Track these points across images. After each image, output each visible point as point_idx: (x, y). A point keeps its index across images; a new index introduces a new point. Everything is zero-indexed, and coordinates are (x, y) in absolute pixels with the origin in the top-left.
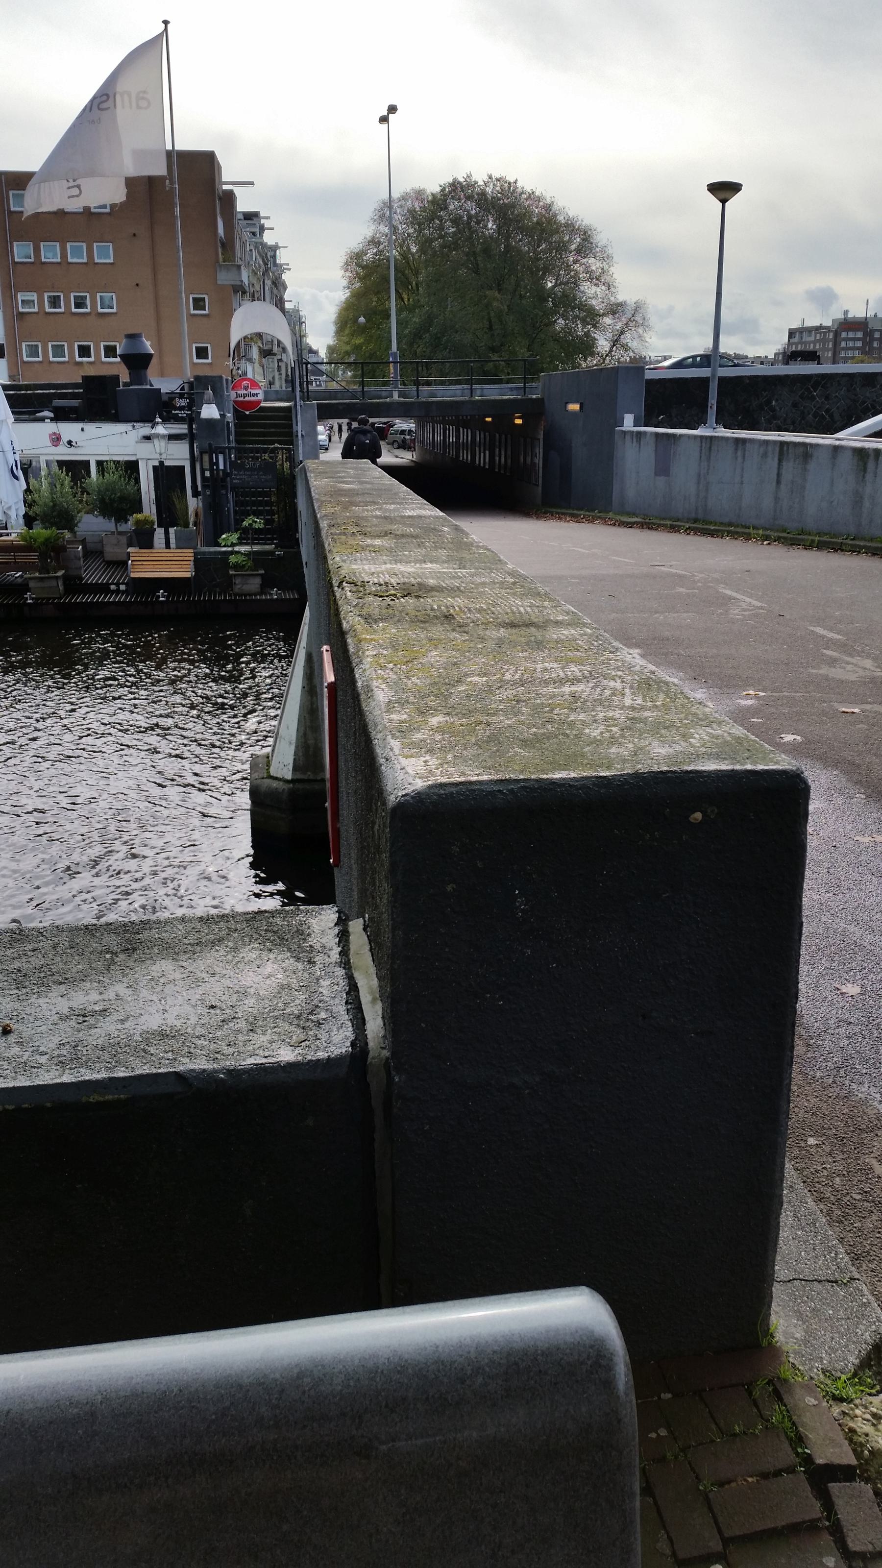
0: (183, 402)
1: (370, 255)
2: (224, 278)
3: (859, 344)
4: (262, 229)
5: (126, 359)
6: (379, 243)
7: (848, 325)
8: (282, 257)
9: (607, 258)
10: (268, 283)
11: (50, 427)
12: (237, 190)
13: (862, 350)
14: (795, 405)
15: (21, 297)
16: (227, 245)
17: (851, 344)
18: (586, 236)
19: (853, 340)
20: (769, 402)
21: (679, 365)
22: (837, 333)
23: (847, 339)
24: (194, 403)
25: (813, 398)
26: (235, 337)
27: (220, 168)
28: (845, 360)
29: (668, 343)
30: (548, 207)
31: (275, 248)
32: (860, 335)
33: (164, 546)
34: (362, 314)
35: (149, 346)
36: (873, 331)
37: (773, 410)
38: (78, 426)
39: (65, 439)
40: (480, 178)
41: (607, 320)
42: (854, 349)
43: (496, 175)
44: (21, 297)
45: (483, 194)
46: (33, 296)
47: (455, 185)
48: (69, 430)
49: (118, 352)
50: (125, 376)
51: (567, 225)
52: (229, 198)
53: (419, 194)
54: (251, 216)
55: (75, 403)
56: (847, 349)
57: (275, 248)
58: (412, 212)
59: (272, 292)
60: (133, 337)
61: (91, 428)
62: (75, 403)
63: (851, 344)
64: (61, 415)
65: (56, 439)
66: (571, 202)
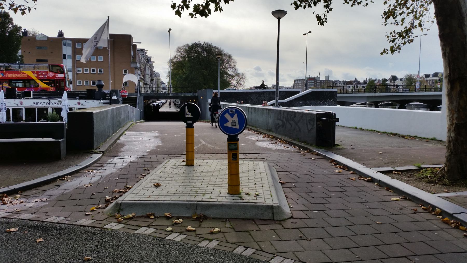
0: (108, 95)
1: (175, 60)
2: (133, 66)
3: (313, 84)
4: (146, 53)
5: (98, 86)
6: (177, 57)
7: (310, 79)
8: (152, 60)
9: (235, 63)
10: (147, 66)
11: (77, 101)
12: (137, 44)
13: (314, 85)
14: (257, 98)
15: (77, 69)
16: (134, 58)
17: (311, 84)
18: (230, 57)
19: (311, 83)
21: (251, 89)
22: (307, 81)
23: (310, 83)
24: (111, 95)
26: (124, 81)
27: (133, 38)
28: (296, 88)
29: (250, 83)
30: (220, 50)
31: (150, 58)
32: (313, 81)
33: (225, 190)
34: (173, 75)
35: (103, 83)
36: (317, 80)
38: (84, 101)
39: (81, 103)
40: (202, 43)
41: (236, 78)
42: (312, 85)
43: (206, 42)
44: (77, 69)
45: (203, 46)
46: (81, 69)
47: (195, 44)
48: (82, 101)
49: (96, 83)
50: (97, 89)
51: (224, 54)
52: (135, 46)
53: (188, 45)
54: (142, 50)
55: (84, 95)
56: (310, 85)
57: (150, 58)
58: (186, 50)
59: (148, 68)
60: (99, 81)
61: (88, 101)
62: (84, 95)
63: (311, 84)
64: (81, 98)
65: (79, 103)
66: (226, 50)
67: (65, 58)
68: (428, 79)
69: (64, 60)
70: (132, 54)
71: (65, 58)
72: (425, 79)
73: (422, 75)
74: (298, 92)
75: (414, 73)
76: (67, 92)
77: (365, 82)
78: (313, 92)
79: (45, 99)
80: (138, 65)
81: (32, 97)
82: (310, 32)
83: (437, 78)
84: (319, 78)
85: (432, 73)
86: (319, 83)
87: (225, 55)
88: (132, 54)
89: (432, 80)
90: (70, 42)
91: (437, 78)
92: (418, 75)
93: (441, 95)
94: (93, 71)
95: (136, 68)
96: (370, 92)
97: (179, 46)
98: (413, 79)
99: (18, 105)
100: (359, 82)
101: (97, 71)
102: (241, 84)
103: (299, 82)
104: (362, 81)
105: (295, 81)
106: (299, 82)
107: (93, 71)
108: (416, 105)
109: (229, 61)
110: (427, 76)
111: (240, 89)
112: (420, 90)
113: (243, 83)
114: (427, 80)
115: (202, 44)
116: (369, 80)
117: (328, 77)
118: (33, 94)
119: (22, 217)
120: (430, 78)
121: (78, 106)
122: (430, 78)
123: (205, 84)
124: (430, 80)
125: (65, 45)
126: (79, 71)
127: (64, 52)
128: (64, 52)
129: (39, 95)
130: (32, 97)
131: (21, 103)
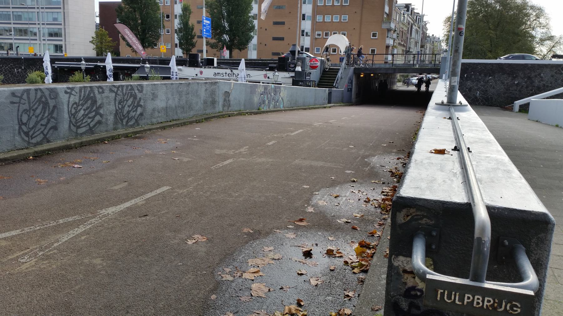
11: (264, 72)
14: (552, 76)
16: (389, 15)
20: (539, 74)
37: (542, 78)
41: (548, 42)
46: (321, 33)
48: (270, 74)
55: (275, 65)
62: (275, 65)
64: (271, 69)
67: (304, 19)
69: (303, 22)
70: (387, 10)
71: (304, 19)
76: (245, 60)
79: (227, 69)
80: (393, 26)
81: (215, 65)
87: (532, 7)
88: (387, 10)
95: (389, 30)
99: (197, 75)
109: (538, 17)
118: (218, 63)
119: (77, 217)
121: (264, 79)
123: (490, 51)
126: (319, 35)
129: (223, 63)
130: (215, 65)
131: (201, 73)
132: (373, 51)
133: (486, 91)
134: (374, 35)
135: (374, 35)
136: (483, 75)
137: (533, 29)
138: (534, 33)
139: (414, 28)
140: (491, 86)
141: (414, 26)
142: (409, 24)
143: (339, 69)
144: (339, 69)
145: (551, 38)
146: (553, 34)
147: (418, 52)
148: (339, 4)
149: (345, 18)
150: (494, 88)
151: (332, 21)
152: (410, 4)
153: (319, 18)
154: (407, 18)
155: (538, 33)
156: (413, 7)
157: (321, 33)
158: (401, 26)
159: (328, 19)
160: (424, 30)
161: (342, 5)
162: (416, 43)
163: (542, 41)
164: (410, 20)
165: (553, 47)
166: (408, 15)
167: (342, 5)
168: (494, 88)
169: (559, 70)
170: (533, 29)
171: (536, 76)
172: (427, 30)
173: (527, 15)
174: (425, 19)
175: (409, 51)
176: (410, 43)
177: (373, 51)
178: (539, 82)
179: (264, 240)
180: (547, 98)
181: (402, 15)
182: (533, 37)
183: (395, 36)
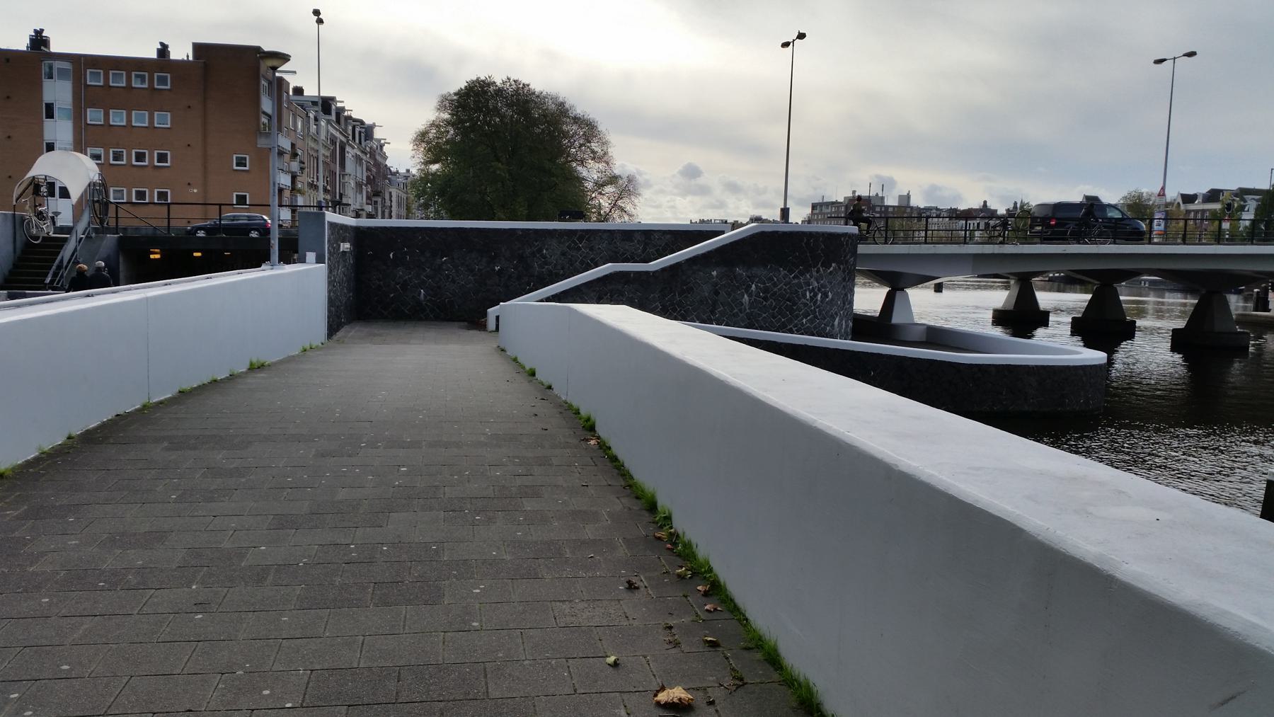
14: (563, 254)
20: (540, 250)
25: (579, 249)
30: (562, 104)
36: (874, 206)
37: (545, 257)
41: (609, 189)
46: (100, 151)
66: (580, 108)
67: (50, 115)
68: (1191, 207)
69: (48, 123)
71: (50, 115)
72: (1183, 207)
73: (1172, 194)
74: (723, 233)
75: (1148, 187)
77: (1010, 213)
78: (763, 233)
82: (801, 36)
83: (1217, 206)
84: (883, 198)
85: (1203, 189)
86: (880, 212)
87: (577, 120)
89: (1204, 211)
90: (66, 65)
91: (1217, 206)
92: (1162, 194)
93: (390, 217)
94: (140, 157)
96: (1046, 240)
97: (445, 92)
98: (1147, 207)
100: (992, 214)
101: (151, 159)
102: (622, 210)
103: (825, 210)
104: (1002, 211)
105: (814, 206)
106: (825, 210)
107: (140, 157)
108: (1151, 282)
110: (1188, 199)
111: (618, 222)
112: (1167, 238)
113: (628, 208)
114: (1188, 212)
115: (499, 82)
116: (1022, 207)
117: (908, 197)
120: (1197, 205)
122: (1197, 205)
124: (1196, 212)
125: (51, 77)
127: (47, 98)
128: (47, 98)
132: (162, 195)
133: (439, 287)
134: (241, 162)
135: (241, 162)
136: (428, 255)
137: (582, 162)
138: (583, 171)
139: (351, 152)
140: (448, 276)
141: (348, 149)
142: (333, 142)
143: (65, 240)
144: (65, 240)
145: (613, 180)
146: (617, 172)
147: (319, 202)
148: (146, 86)
149: (163, 120)
150: (454, 281)
151: (151, 127)
152: (333, 99)
153: (94, 116)
154: (325, 127)
155: (590, 172)
156: (339, 105)
157: (100, 151)
158: (312, 144)
159: (140, 119)
160: (378, 158)
161: (152, 89)
162: (359, 185)
163: (600, 185)
164: (338, 134)
165: (620, 198)
166: (328, 122)
167: (152, 89)
168: (454, 281)
169: (574, 242)
170: (582, 162)
171: (533, 254)
172: (385, 158)
173: (566, 135)
174: (377, 134)
175: (339, 203)
176: (343, 185)
177: (162, 195)
178: (541, 266)
179: (1156, 438)
180: (548, 300)
181: (312, 121)
182: (580, 180)
183: (295, 166)
